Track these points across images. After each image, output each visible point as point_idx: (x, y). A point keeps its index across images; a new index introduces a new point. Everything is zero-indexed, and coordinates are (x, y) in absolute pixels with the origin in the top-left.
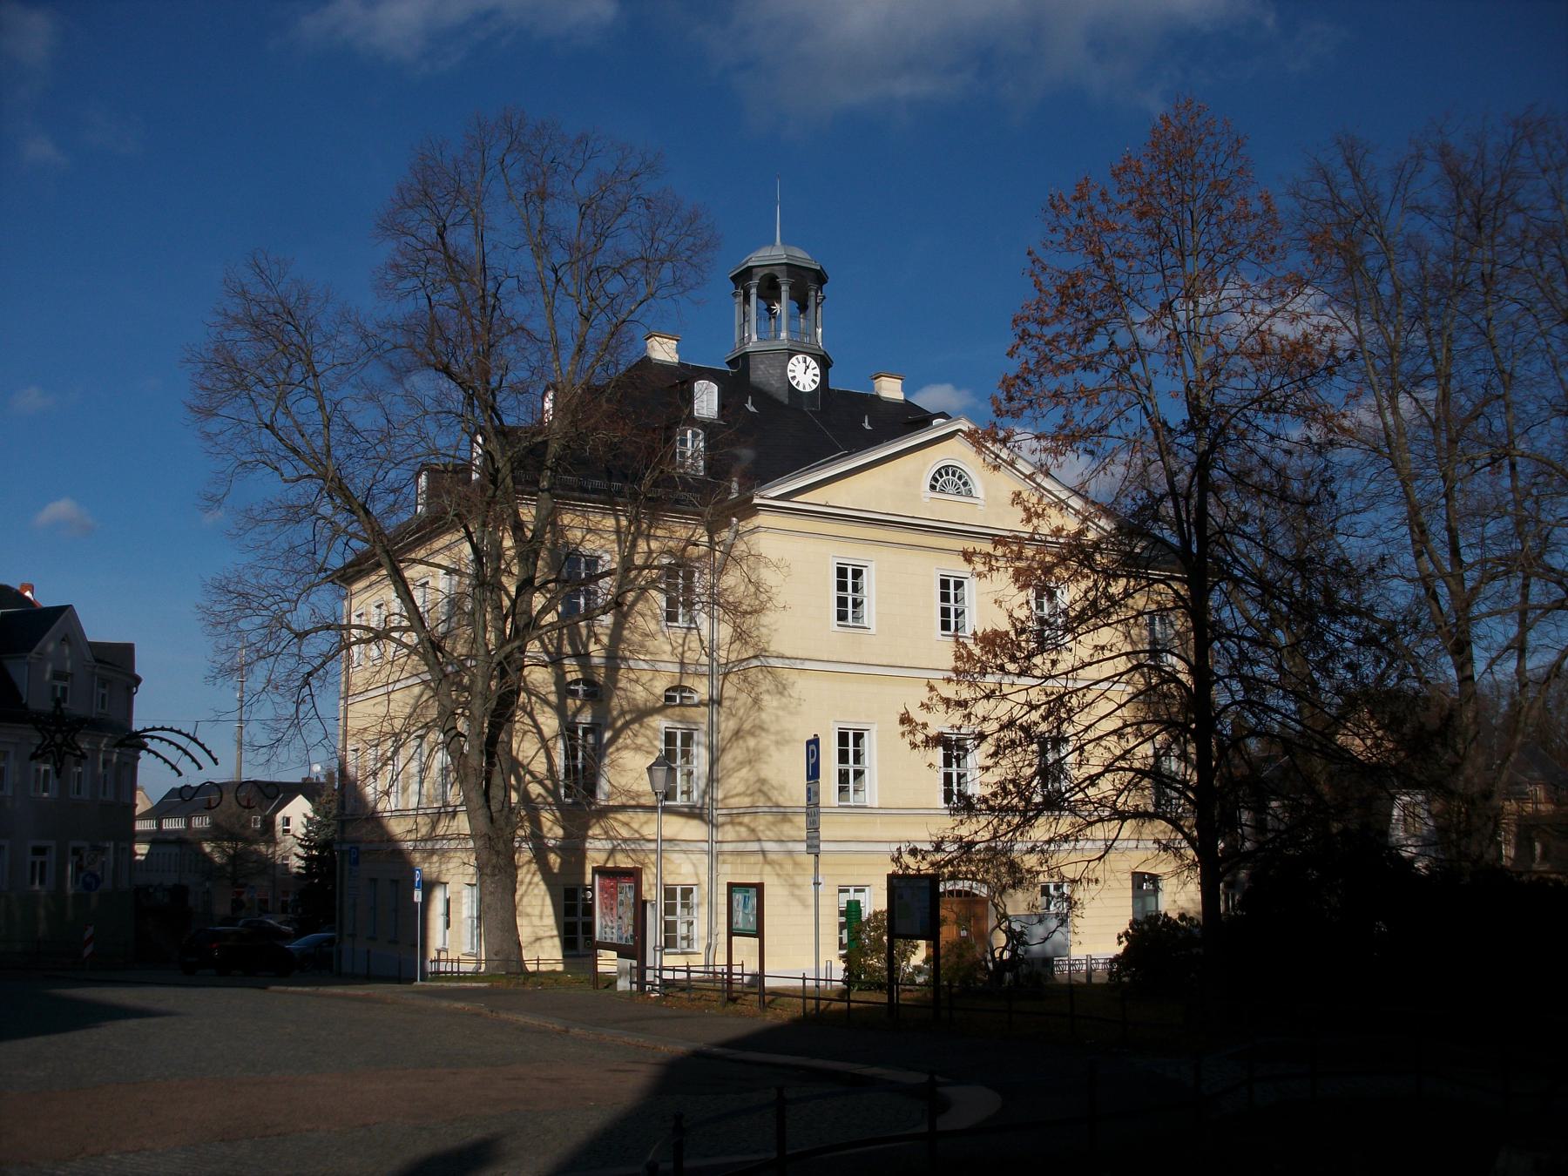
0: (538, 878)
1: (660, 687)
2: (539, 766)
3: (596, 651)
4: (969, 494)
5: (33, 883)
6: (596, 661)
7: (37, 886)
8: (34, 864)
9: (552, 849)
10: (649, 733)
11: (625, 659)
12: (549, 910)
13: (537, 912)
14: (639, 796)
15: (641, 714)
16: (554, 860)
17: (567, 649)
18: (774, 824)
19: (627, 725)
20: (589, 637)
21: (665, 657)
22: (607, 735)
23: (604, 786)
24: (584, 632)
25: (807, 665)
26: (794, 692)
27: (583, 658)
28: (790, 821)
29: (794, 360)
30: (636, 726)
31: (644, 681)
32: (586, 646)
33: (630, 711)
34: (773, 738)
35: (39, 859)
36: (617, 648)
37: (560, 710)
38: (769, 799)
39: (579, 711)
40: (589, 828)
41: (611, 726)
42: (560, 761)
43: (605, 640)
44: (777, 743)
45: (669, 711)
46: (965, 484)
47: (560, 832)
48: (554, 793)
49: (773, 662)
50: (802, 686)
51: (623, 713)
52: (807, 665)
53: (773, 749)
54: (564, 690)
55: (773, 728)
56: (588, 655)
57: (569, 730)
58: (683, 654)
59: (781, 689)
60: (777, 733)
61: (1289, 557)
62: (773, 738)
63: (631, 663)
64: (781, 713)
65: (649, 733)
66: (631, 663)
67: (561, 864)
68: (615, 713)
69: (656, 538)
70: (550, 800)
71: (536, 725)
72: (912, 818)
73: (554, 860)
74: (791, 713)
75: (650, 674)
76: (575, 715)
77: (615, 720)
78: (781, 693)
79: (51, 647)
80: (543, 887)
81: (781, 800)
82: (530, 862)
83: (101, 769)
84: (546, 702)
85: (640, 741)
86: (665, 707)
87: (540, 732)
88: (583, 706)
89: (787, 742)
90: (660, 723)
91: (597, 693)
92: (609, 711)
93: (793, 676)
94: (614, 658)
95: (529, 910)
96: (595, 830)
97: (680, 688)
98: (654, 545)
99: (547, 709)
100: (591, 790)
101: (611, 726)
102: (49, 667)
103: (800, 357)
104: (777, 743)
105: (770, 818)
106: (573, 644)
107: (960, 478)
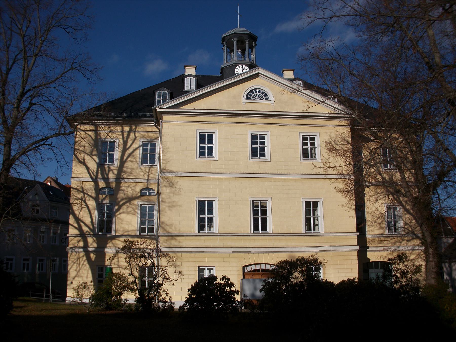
0: (86, 263)
1: (138, 189)
2: (87, 220)
3: (111, 176)
4: (267, 99)
5: (24, 269)
6: (111, 180)
7: (25, 271)
8: (24, 264)
9: (92, 252)
10: (134, 207)
11: (123, 179)
12: (90, 275)
13: (85, 275)
14: (128, 231)
15: (130, 200)
16: (92, 256)
17: (100, 176)
18: (167, 240)
19: (124, 204)
20: (109, 171)
21: (141, 177)
22: (116, 208)
23: (114, 227)
24: (107, 169)
25: (183, 174)
26: (178, 186)
27: (106, 180)
28: (175, 239)
29: (238, 67)
30: (128, 204)
31: (130, 188)
32: (108, 175)
33: (126, 199)
34: (167, 205)
35: (26, 263)
36: (121, 175)
37: (96, 199)
38: (165, 230)
39: (104, 199)
40: (107, 244)
41: (118, 204)
42: (96, 220)
43: (116, 172)
44: (169, 207)
45: (142, 198)
46: (263, 93)
47: (95, 245)
48: (93, 230)
49: (167, 174)
50: (181, 183)
51: (122, 200)
52: (183, 174)
53: (167, 209)
54: (98, 190)
55: (167, 201)
56: (108, 178)
57: (100, 206)
58: (149, 175)
59: (172, 185)
60: (169, 203)
61: (293, 77)
62: (167, 205)
63: (126, 180)
64: (172, 195)
65: (134, 207)
66: (126, 180)
67: (96, 258)
68: (119, 200)
69: (138, 132)
70: (92, 233)
71: (87, 205)
72: (235, 238)
73: (92, 256)
74: (176, 194)
75: (134, 184)
76: (102, 201)
77: (119, 202)
78: (171, 187)
79: (31, 197)
80: (88, 266)
81: (170, 230)
82: (83, 256)
83: (52, 234)
84: (91, 196)
85: (130, 209)
86: (141, 196)
87: (88, 208)
88: (106, 197)
89: (174, 206)
90: (138, 202)
91: (113, 192)
92: (117, 199)
93: (177, 179)
94: (119, 179)
95: (82, 275)
96: (110, 245)
97: (148, 189)
98: (137, 135)
99: (91, 199)
100: (109, 230)
101: (118, 204)
102: (30, 203)
103: (241, 66)
104: (169, 207)
105: (165, 238)
106: (102, 174)
107: (259, 92)
